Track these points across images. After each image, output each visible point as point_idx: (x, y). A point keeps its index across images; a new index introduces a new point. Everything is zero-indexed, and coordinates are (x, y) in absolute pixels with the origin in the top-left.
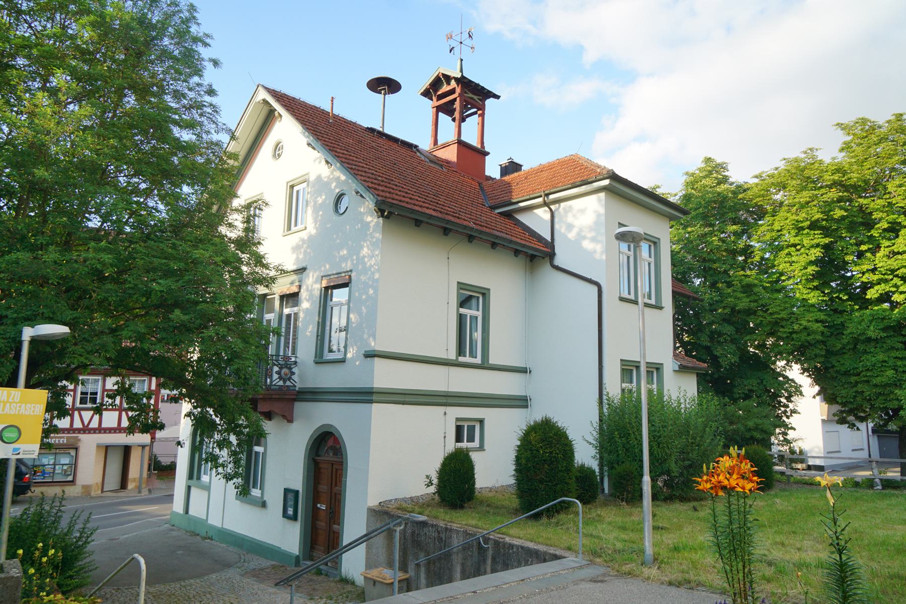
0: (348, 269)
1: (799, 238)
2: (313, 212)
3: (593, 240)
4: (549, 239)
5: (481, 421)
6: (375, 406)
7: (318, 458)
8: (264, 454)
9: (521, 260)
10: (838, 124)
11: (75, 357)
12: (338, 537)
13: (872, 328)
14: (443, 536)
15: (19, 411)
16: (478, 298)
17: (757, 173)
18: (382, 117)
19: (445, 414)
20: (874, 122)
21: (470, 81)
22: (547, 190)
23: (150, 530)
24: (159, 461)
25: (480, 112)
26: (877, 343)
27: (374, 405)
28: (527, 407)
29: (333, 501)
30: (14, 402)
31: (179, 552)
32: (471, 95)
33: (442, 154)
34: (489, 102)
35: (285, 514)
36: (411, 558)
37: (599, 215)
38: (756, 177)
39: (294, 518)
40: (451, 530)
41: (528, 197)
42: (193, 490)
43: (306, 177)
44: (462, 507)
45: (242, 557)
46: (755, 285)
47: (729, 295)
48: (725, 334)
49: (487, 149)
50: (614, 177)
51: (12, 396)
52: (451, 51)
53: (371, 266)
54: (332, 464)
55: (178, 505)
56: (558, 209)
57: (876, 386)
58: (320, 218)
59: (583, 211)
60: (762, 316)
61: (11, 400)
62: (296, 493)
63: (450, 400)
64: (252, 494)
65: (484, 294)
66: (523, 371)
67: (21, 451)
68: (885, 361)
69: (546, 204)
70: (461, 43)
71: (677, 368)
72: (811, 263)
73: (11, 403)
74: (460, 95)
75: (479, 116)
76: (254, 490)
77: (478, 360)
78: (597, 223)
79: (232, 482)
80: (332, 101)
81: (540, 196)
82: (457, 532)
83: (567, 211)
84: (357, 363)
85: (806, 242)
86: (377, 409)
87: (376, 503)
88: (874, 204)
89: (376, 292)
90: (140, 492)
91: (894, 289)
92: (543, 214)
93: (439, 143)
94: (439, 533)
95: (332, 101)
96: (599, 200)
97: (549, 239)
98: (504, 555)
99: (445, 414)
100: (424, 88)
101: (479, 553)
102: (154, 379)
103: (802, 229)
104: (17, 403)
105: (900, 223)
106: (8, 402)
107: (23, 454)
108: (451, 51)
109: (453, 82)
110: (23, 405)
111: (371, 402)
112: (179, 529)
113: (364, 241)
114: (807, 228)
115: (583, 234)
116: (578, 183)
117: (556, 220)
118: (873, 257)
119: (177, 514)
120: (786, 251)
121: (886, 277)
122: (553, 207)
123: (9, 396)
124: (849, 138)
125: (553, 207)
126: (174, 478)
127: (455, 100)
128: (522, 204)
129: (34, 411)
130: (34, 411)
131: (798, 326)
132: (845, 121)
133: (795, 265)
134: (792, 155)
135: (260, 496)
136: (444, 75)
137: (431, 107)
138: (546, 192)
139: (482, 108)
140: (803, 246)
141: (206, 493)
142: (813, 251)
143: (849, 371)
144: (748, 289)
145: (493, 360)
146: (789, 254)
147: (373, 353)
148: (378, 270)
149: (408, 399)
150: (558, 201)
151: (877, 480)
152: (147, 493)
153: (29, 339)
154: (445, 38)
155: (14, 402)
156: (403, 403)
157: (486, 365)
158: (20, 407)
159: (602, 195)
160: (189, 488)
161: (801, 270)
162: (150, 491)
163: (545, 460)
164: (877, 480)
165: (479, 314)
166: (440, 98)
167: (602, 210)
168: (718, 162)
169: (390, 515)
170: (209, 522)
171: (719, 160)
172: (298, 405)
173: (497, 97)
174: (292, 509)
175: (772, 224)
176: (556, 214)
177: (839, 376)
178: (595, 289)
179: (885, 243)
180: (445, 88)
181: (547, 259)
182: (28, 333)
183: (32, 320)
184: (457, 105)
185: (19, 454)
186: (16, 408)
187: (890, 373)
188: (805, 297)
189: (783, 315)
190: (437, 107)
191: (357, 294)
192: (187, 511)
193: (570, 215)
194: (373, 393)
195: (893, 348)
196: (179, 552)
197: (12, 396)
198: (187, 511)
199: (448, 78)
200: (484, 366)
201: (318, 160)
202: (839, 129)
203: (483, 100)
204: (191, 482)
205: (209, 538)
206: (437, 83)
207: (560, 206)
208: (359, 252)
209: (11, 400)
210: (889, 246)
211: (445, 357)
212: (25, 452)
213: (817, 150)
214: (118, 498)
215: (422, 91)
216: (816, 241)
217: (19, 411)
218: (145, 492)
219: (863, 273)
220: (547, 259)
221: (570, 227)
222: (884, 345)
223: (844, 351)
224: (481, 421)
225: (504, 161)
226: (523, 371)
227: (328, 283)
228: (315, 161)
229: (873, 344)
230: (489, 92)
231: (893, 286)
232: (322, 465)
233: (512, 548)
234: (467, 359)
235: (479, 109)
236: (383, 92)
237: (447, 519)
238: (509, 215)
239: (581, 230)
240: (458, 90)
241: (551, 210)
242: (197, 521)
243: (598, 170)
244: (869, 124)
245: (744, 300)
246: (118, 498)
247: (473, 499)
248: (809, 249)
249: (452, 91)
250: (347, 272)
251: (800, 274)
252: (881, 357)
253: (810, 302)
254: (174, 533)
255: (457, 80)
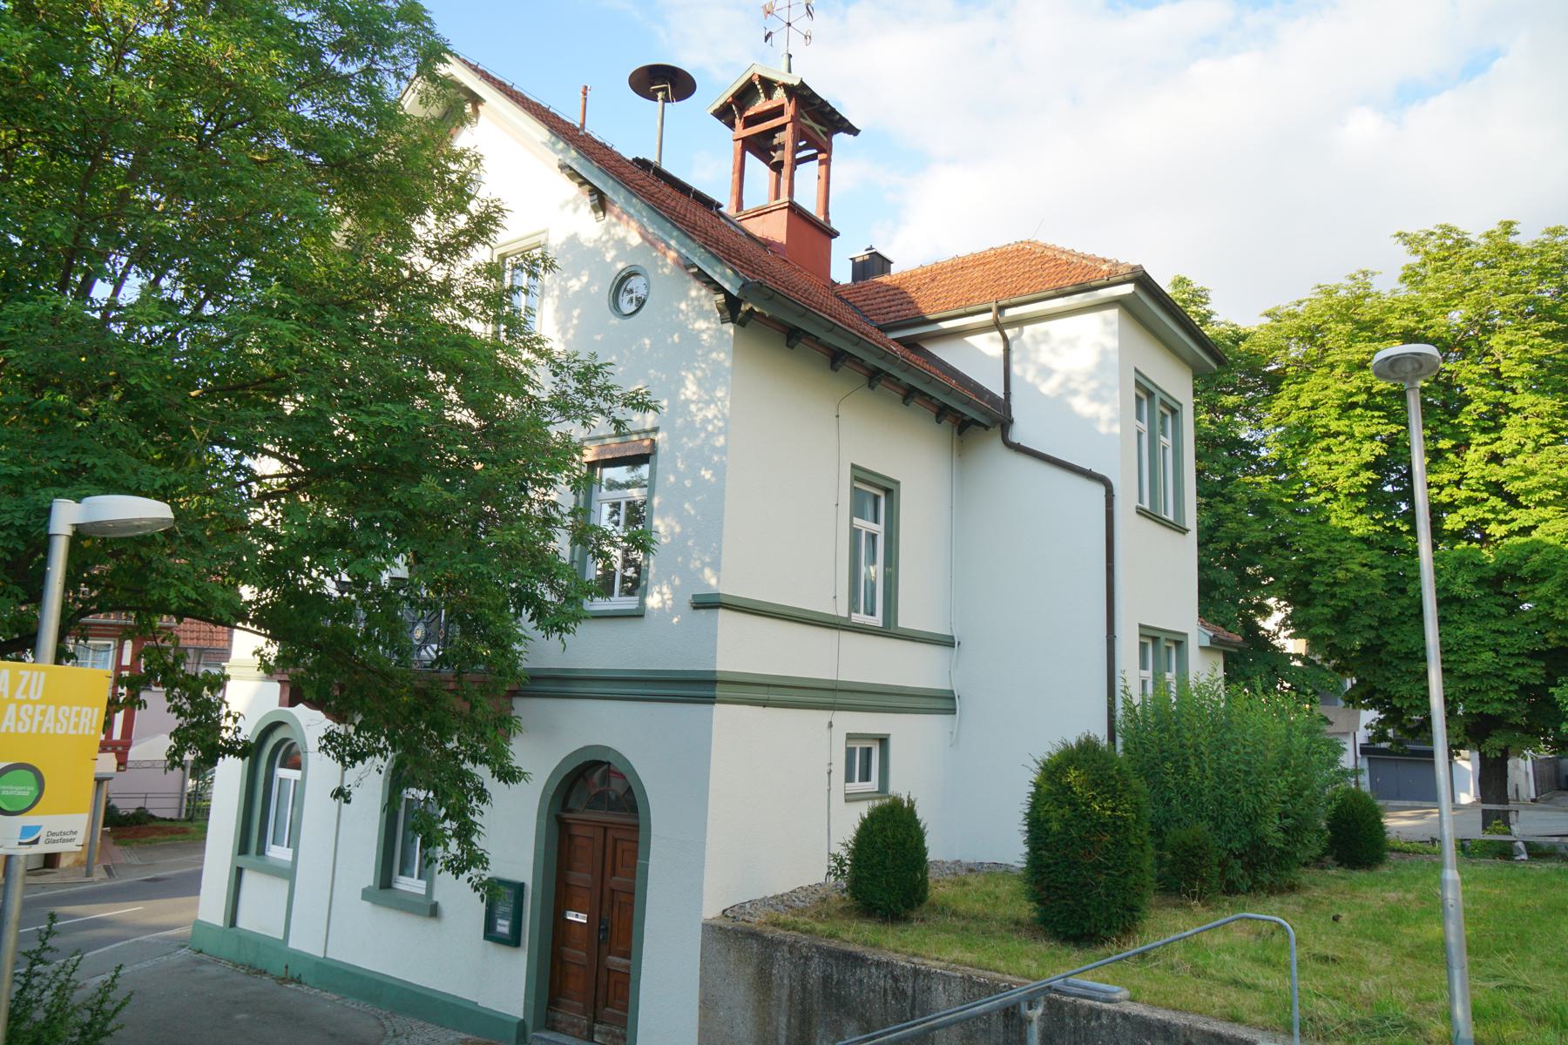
0: (648, 427)
1: (1342, 423)
2: (557, 311)
3: (1095, 397)
4: (1000, 393)
5: (883, 741)
6: (719, 709)
7: (567, 815)
8: (300, 786)
9: (945, 430)
10: (1399, 235)
11: (169, 586)
12: (626, 985)
13: (1459, 581)
14: (908, 987)
15: (41, 724)
16: (876, 498)
17: (1269, 308)
18: (658, 143)
19: (831, 725)
20: (1464, 233)
21: (814, 95)
22: (1001, 298)
23: (150, 963)
24: (113, 807)
25: (822, 156)
26: (1463, 606)
27: (717, 706)
28: (953, 711)
29: (606, 906)
30: (28, 701)
31: (239, 1017)
32: (809, 122)
33: (757, 227)
34: (840, 140)
35: (490, 933)
36: (821, 1031)
37: (1104, 352)
38: (1268, 315)
39: (514, 940)
40: (928, 975)
41: (961, 311)
42: (248, 877)
43: (542, 238)
44: (906, 919)
45: (386, 1023)
46: (1270, 501)
47: (1228, 517)
48: (1224, 585)
49: (834, 225)
50: (1143, 281)
51: (22, 686)
52: (766, 39)
53: (706, 421)
54: (605, 828)
55: (210, 906)
56: (1018, 336)
57: (1466, 676)
58: (575, 321)
59: (1071, 342)
60: (1281, 556)
61: (19, 696)
62: (519, 888)
63: (843, 699)
64: (399, 886)
65: (888, 491)
66: (948, 642)
67: (42, 833)
68: (1478, 637)
69: (998, 326)
70: (789, 24)
71: (1207, 643)
72: (1367, 466)
73: (20, 703)
74: (793, 119)
75: (821, 163)
76: (403, 879)
77: (877, 620)
78: (1102, 366)
79: (467, 875)
80: (585, 94)
81: (989, 310)
82: (947, 980)
83: (1036, 342)
84: (675, 620)
85: (1358, 430)
86: (723, 715)
87: (717, 912)
88: (1465, 371)
89: (719, 471)
90: (88, 874)
91: (1490, 516)
92: (988, 345)
93: (747, 206)
94: (896, 979)
95: (585, 94)
96: (1107, 323)
97: (1000, 393)
98: (1075, 1031)
99: (831, 725)
100: (721, 101)
101: (1006, 1026)
102: (128, 645)
103: (1354, 405)
104: (35, 703)
105: (1507, 404)
106: (12, 699)
107: (48, 842)
108: (766, 39)
109: (779, 96)
110: (52, 709)
111: (711, 700)
112: (217, 960)
113: (688, 369)
114: (1362, 407)
115: (1072, 385)
116: (1069, 289)
117: (1014, 357)
118: (1459, 460)
119: (209, 927)
120: (1324, 444)
121: (1478, 494)
122: (1009, 333)
123: (15, 682)
124: (1417, 260)
125: (1009, 333)
126: (204, 848)
127: (782, 128)
128: (945, 325)
129: (76, 726)
130: (76, 726)
131: (1343, 572)
132: (1413, 229)
133: (1337, 470)
134: (1330, 281)
135: (423, 892)
136: (763, 80)
137: (731, 138)
138: (1001, 303)
139: (826, 149)
140: (1352, 436)
141: (285, 885)
142: (1367, 445)
143: (1415, 653)
144: (1261, 507)
145: (905, 621)
146: (1328, 449)
147: (712, 600)
148: (721, 431)
149: (774, 695)
150: (1019, 322)
151: (1520, 844)
152: (104, 875)
153: (69, 531)
154: (762, 13)
155: (28, 701)
156: (765, 704)
157: (892, 630)
158: (43, 713)
159: (1113, 314)
160: (239, 872)
161: (1349, 477)
162: (108, 869)
163: (1104, 825)
164: (1520, 844)
165: (879, 529)
166: (750, 122)
167: (1112, 343)
168: (1195, 286)
169: (764, 939)
170: (293, 944)
171: (1197, 284)
172: (524, 708)
173: (853, 131)
174: (506, 923)
175: (1296, 398)
176: (1014, 346)
177: (1396, 662)
178: (1100, 490)
179: (1478, 438)
180: (761, 105)
181: (997, 430)
182: (66, 515)
183: (78, 481)
184: (785, 137)
185: (36, 842)
186: (32, 718)
187: (1488, 656)
188: (1347, 524)
189: (1320, 553)
190: (744, 140)
191: (672, 479)
192: (232, 919)
193: (1044, 348)
194: (715, 682)
195: (1491, 615)
196: (239, 1017)
197: (22, 686)
198: (232, 919)
199: (769, 86)
200: (889, 631)
201: (571, 206)
202: (1401, 242)
203: (829, 135)
204: (243, 861)
205: (292, 980)
206: (746, 94)
207: (1021, 332)
208: (677, 393)
209: (19, 696)
210: (1486, 444)
211: (832, 612)
212: (53, 837)
213: (1373, 274)
214: (44, 887)
215: (717, 106)
216: (1373, 430)
217: (41, 724)
218: (99, 874)
219: (1441, 488)
220: (997, 430)
221: (1046, 372)
222: (1476, 610)
223: (1402, 618)
224: (883, 741)
225: (860, 253)
226: (948, 642)
227: (598, 454)
228: (562, 207)
229: (1456, 607)
230: (843, 120)
231: (1488, 511)
232: (575, 831)
233: (1099, 1017)
234: (860, 618)
235: (821, 151)
236: (660, 95)
237: (859, 936)
238: (912, 344)
239: (1068, 379)
240: (790, 110)
241: (1005, 338)
242: (259, 942)
243: (1105, 267)
244: (1455, 236)
245: (1256, 526)
246: (44, 887)
247: (921, 901)
248: (1360, 442)
249: (778, 112)
250: (646, 432)
251: (1346, 484)
252: (1471, 629)
253: (1354, 533)
254: (211, 970)
255: (790, 90)
